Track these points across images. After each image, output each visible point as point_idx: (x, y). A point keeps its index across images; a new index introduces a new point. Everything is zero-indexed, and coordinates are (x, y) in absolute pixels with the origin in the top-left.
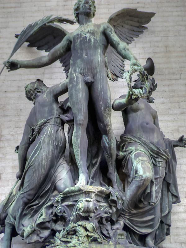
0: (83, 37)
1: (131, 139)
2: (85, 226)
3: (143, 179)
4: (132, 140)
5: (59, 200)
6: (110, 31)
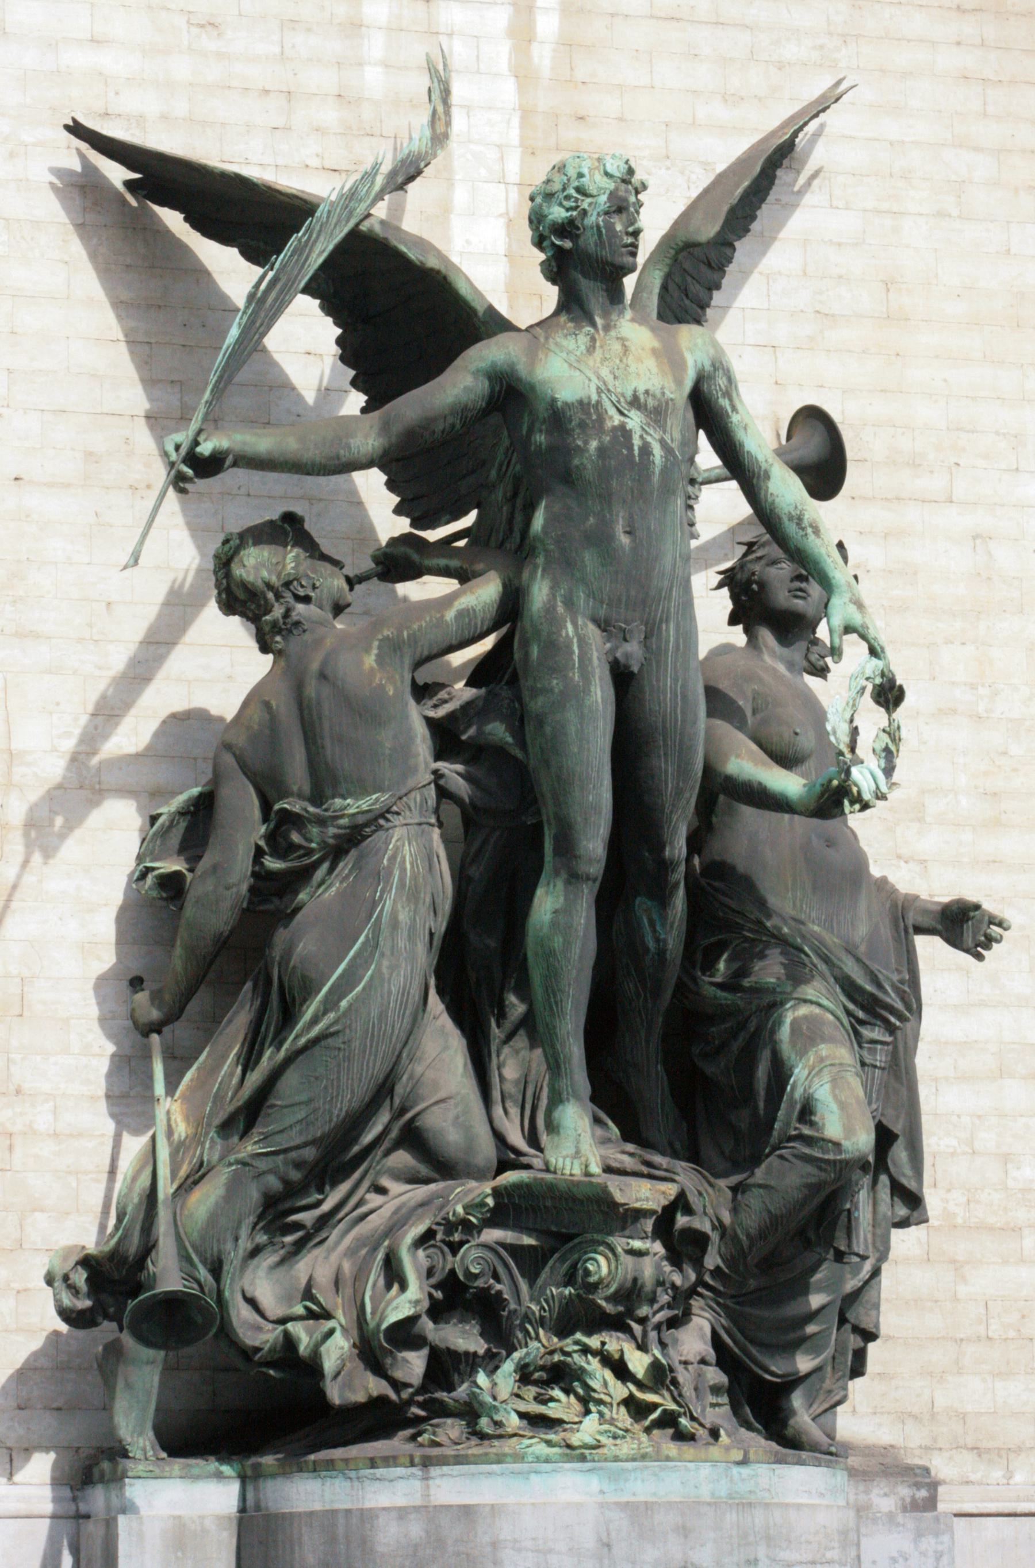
0: (614, 429)
3: (841, 1161)
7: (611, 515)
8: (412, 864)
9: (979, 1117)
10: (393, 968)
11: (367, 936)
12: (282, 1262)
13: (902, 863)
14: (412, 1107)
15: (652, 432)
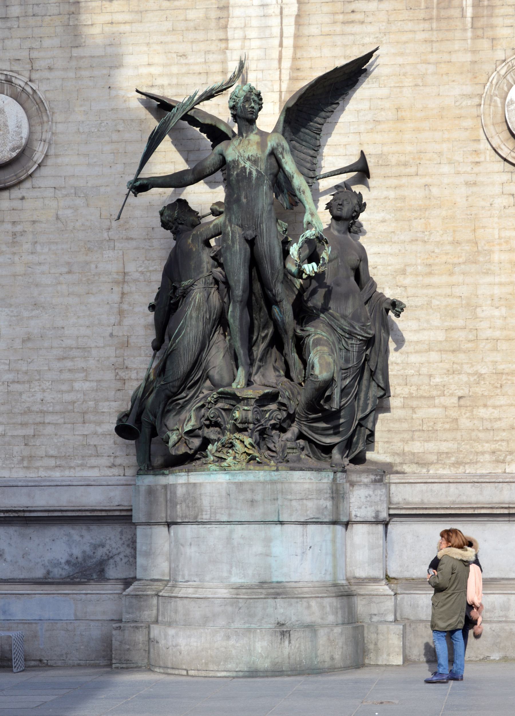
0: (242, 167)
6: (282, 153)
8: (198, 300)
9: (422, 364)
10: (190, 330)
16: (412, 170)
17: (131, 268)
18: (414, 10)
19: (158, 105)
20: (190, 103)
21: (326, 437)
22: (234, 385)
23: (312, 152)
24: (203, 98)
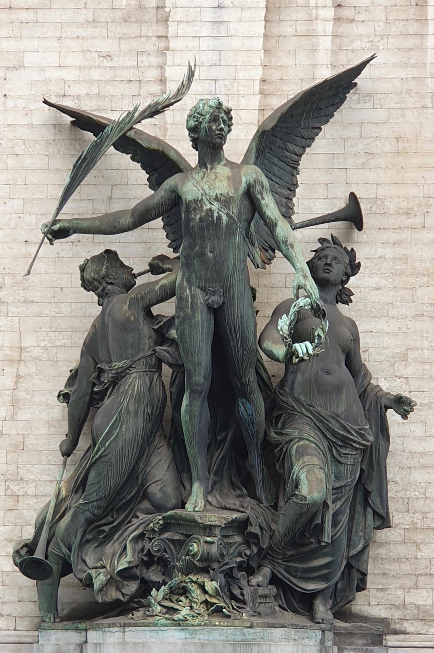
0: (207, 210)
1: (293, 407)
2: (202, 584)
4: (295, 409)
5: (155, 528)
7: (205, 245)
8: (138, 388)
9: (429, 483)
11: (117, 417)
12: (98, 546)
13: (397, 379)
14: (146, 484)
15: (223, 210)
16: (417, 221)
17: (29, 341)
18: (421, 6)
19: (72, 122)
20: (130, 120)
21: (306, 582)
22: (189, 506)
23: (286, 192)
24: (146, 114)
